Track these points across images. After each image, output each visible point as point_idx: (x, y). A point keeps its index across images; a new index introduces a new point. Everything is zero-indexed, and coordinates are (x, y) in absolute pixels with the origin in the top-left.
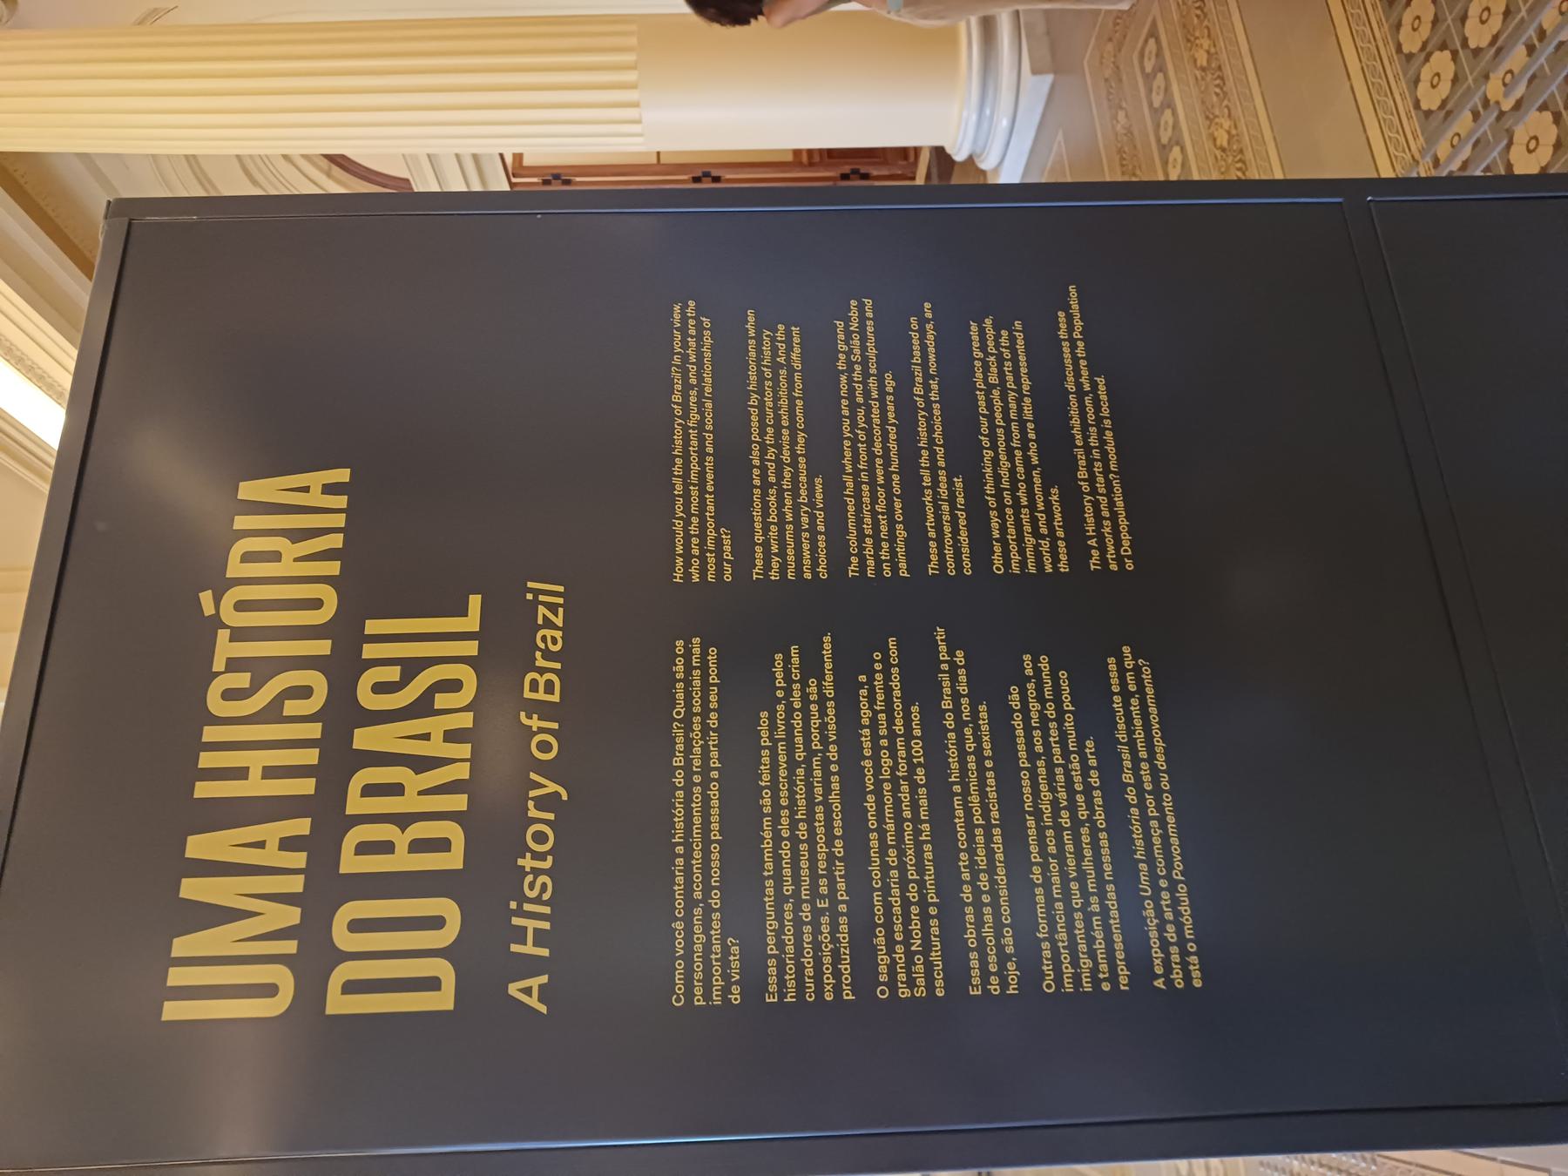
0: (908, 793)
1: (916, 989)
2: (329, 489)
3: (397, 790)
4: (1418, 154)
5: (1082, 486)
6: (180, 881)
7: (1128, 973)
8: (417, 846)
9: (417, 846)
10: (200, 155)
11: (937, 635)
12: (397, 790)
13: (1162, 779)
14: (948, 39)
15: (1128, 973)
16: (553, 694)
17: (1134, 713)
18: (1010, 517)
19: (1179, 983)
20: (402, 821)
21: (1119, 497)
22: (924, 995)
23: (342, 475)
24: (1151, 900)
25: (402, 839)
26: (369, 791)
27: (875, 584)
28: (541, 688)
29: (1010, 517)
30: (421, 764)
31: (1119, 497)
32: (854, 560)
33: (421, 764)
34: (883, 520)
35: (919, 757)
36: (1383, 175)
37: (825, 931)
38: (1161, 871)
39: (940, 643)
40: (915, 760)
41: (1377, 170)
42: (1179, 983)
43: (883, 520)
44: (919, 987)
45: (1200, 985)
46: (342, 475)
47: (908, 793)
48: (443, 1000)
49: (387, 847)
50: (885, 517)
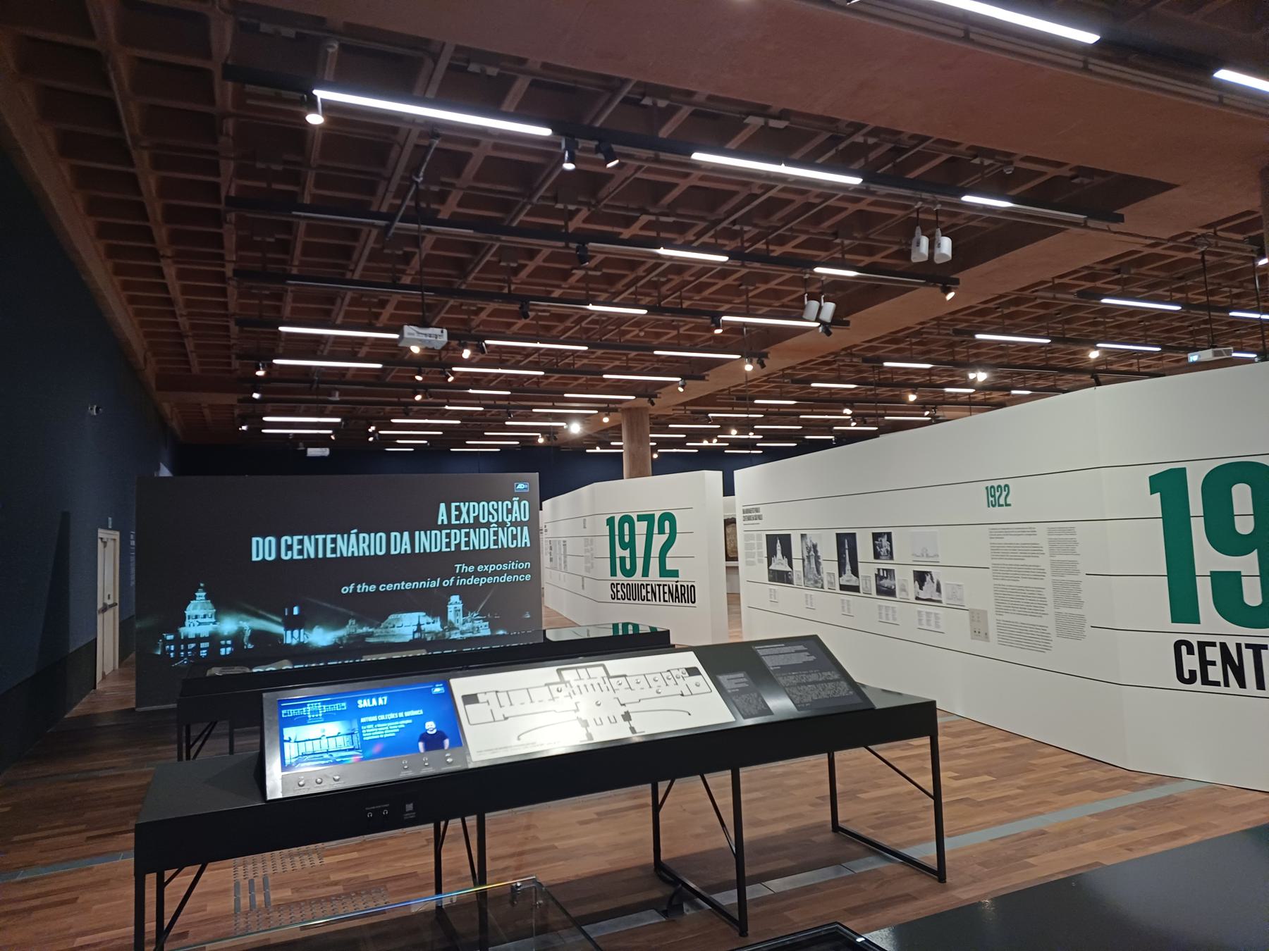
0: (480, 578)
2: (526, 543)
4: (636, 800)
5: (449, 580)
7: (481, 585)
10: (735, 527)
11: (515, 563)
13: (464, 584)
14: (348, 639)
15: (481, 585)
16: (643, 576)
17: (399, 584)
18: (522, 578)
19: (345, 590)
21: (514, 566)
23: (528, 545)
24: (379, 586)
29: (522, 578)
31: (514, 566)
32: (471, 569)
38: (383, 588)
41: (550, 690)
42: (345, 590)
45: (343, 591)
46: (528, 545)
47: (480, 578)
48: (254, 558)
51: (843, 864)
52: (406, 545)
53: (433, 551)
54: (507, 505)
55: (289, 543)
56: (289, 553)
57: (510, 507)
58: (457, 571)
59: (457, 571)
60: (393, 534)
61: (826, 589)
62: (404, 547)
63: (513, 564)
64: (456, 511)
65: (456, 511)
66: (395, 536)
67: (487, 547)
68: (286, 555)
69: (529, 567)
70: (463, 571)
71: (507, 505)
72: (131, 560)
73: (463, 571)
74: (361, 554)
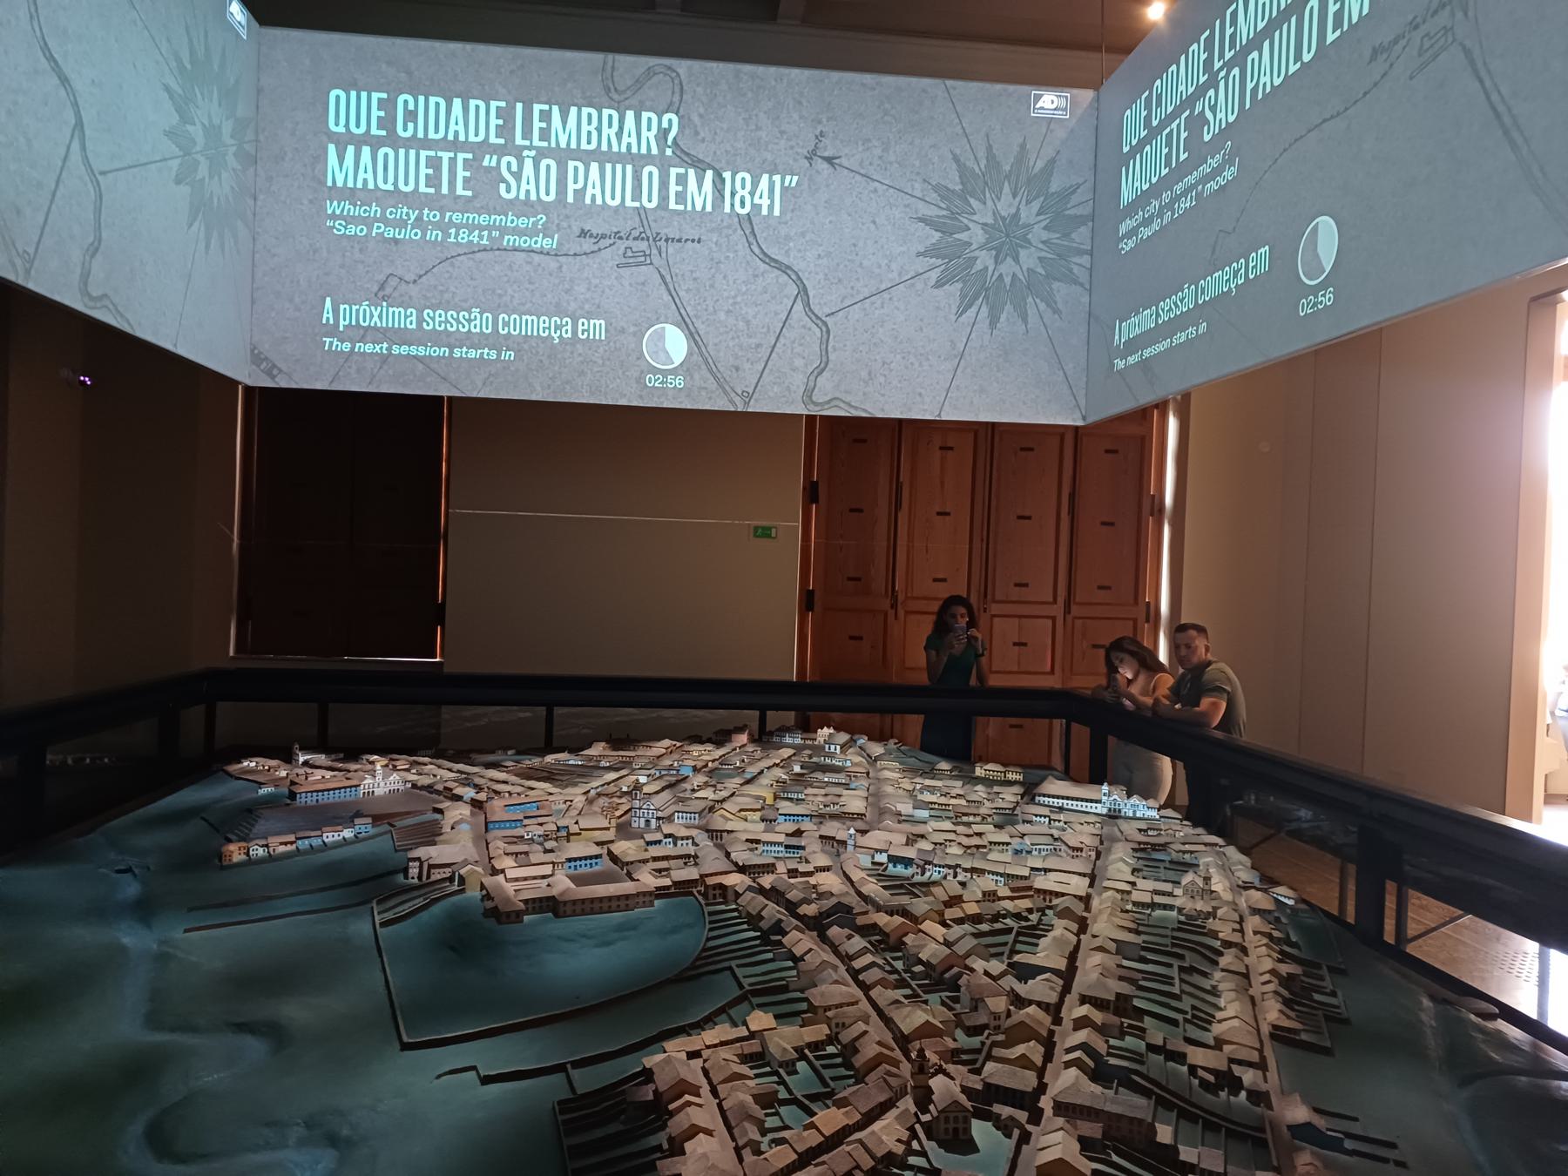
1: (344, 223)
3: (610, 126)
6: (1160, 1143)
8: (589, 133)
9: (589, 133)
12: (610, 126)
20: (599, 130)
22: (335, 231)
25: (592, 128)
26: (610, 116)
27: (106, 760)
28: (951, 1119)
30: (619, 134)
33: (619, 134)
34: (381, 348)
35: (456, 238)
36: (1532, 947)
37: (520, 221)
39: (479, 351)
40: (453, 231)
43: (381, 348)
44: (334, 227)
49: (590, 123)
50: (385, 352)
51: (194, 151)
52: (457, 124)
53: (470, 140)
54: (406, 102)
55: (411, 107)
56: (665, 125)
57: (411, 107)
58: (326, 348)
59: (326, 348)
60: (473, 103)
61: (567, 1142)
62: (452, 127)
63: (405, 210)
64: (379, 109)
65: (379, 109)
66: (477, 107)
67: (481, 137)
68: (405, 129)
69: (512, 358)
70: (334, 349)
71: (406, 102)
72: (739, 182)
73: (334, 349)
74: (644, 151)
